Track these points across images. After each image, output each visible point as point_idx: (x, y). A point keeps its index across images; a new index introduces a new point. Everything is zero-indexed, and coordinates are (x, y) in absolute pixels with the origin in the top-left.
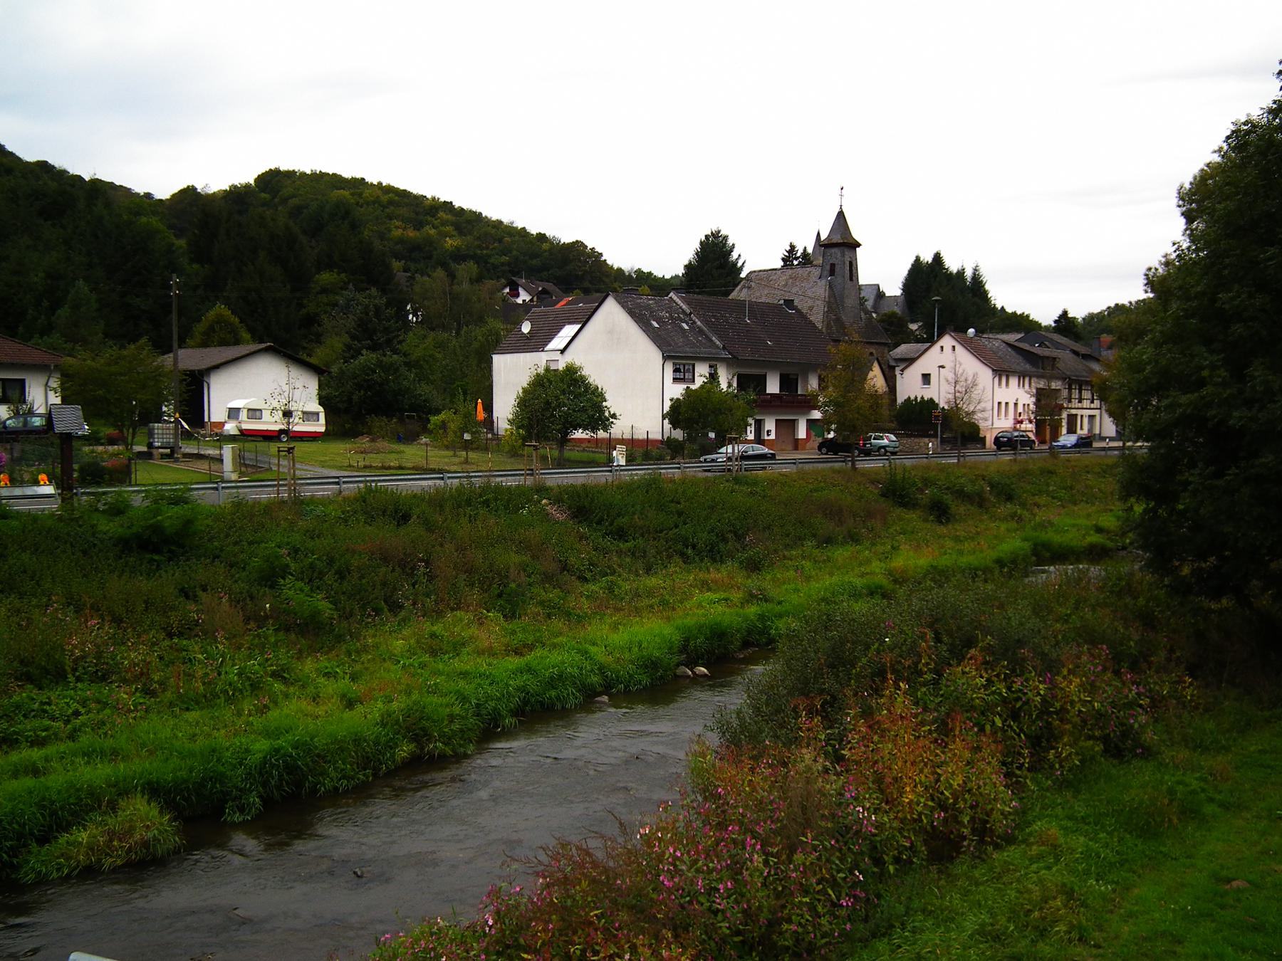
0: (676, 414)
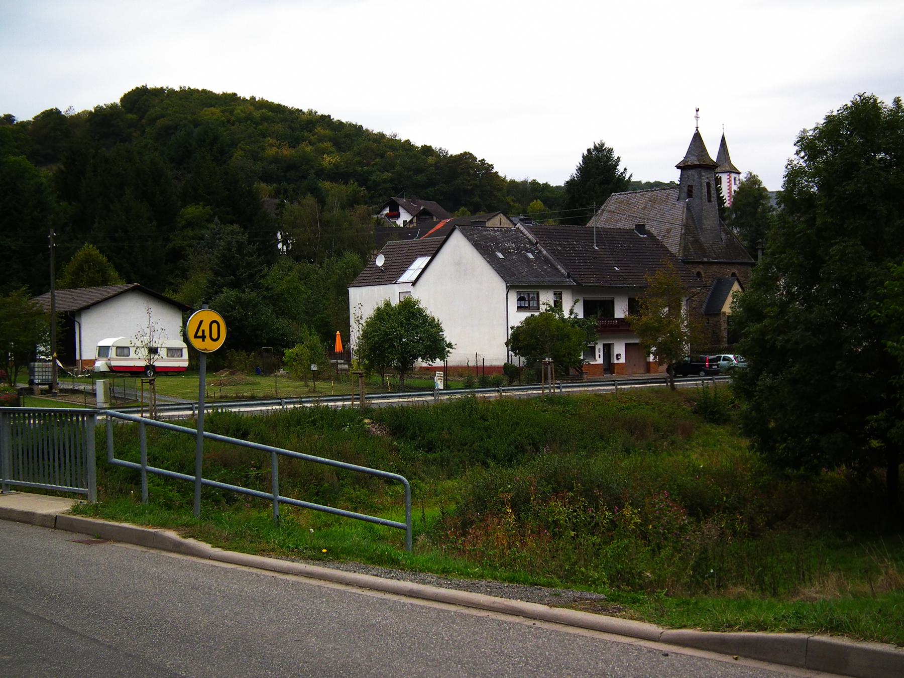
0: (518, 341)
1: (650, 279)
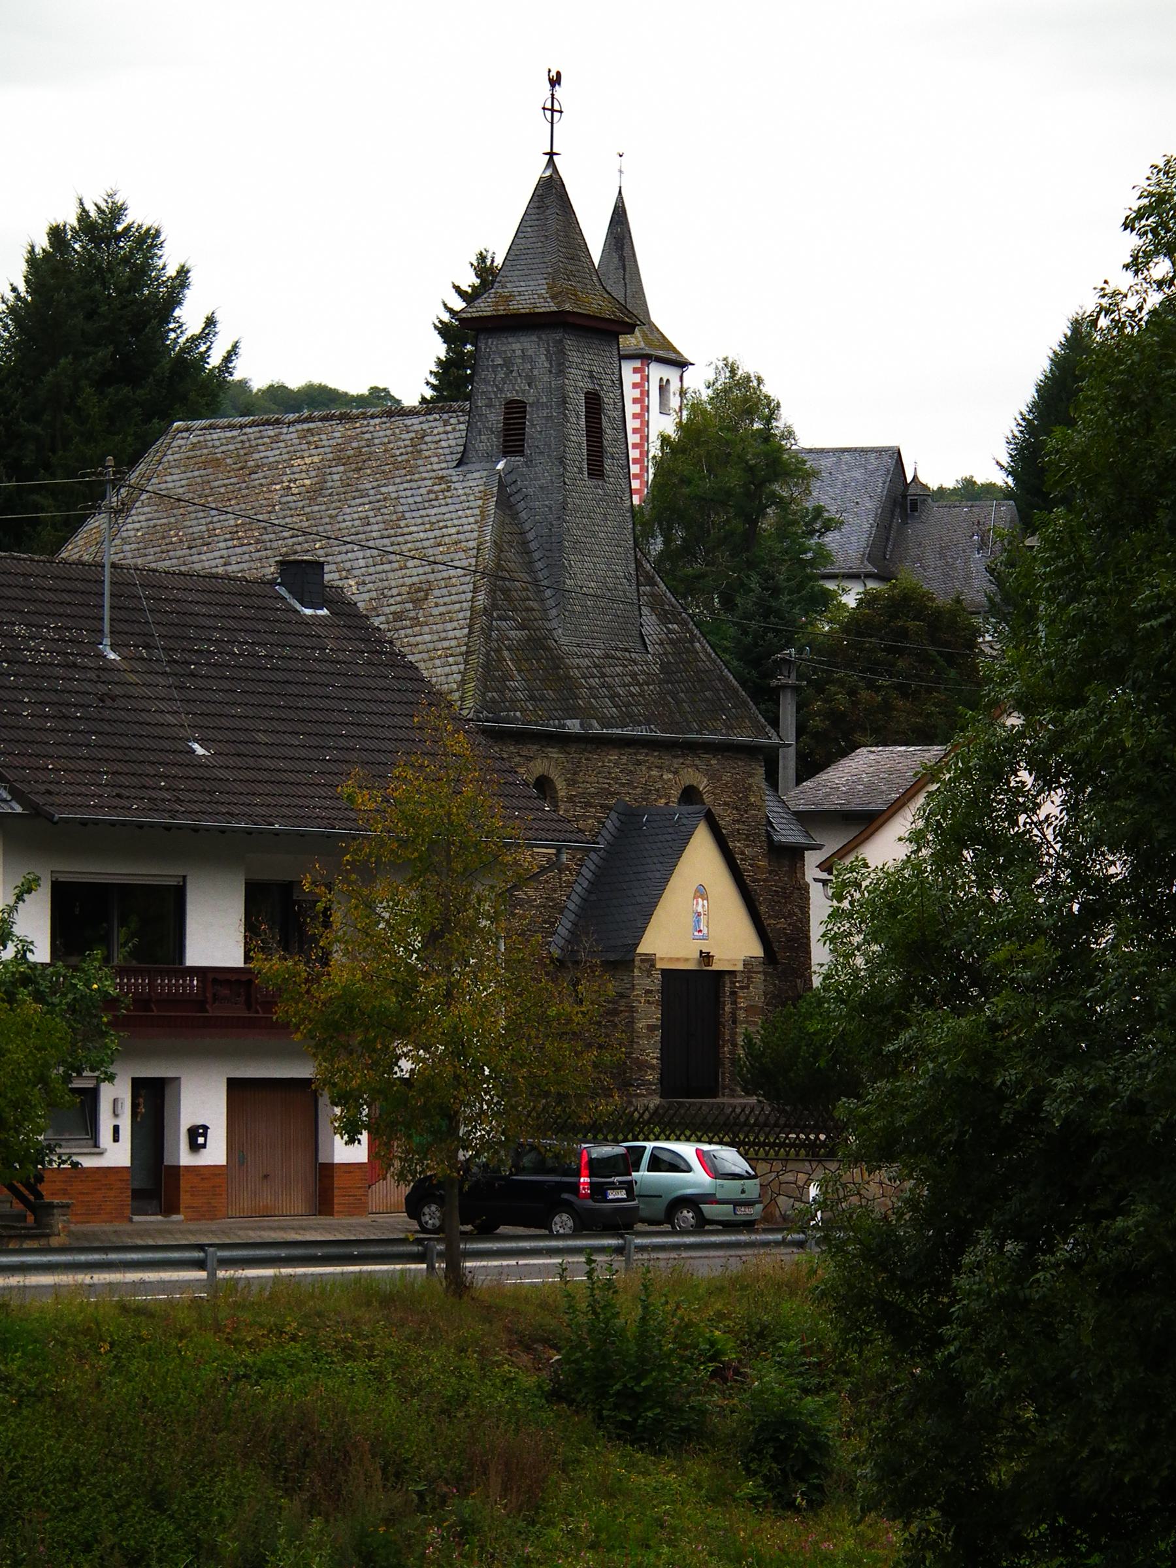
1: (365, 801)
